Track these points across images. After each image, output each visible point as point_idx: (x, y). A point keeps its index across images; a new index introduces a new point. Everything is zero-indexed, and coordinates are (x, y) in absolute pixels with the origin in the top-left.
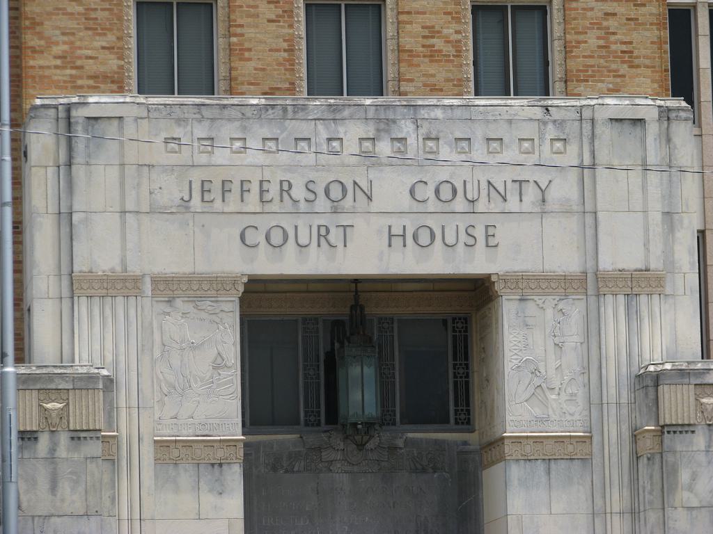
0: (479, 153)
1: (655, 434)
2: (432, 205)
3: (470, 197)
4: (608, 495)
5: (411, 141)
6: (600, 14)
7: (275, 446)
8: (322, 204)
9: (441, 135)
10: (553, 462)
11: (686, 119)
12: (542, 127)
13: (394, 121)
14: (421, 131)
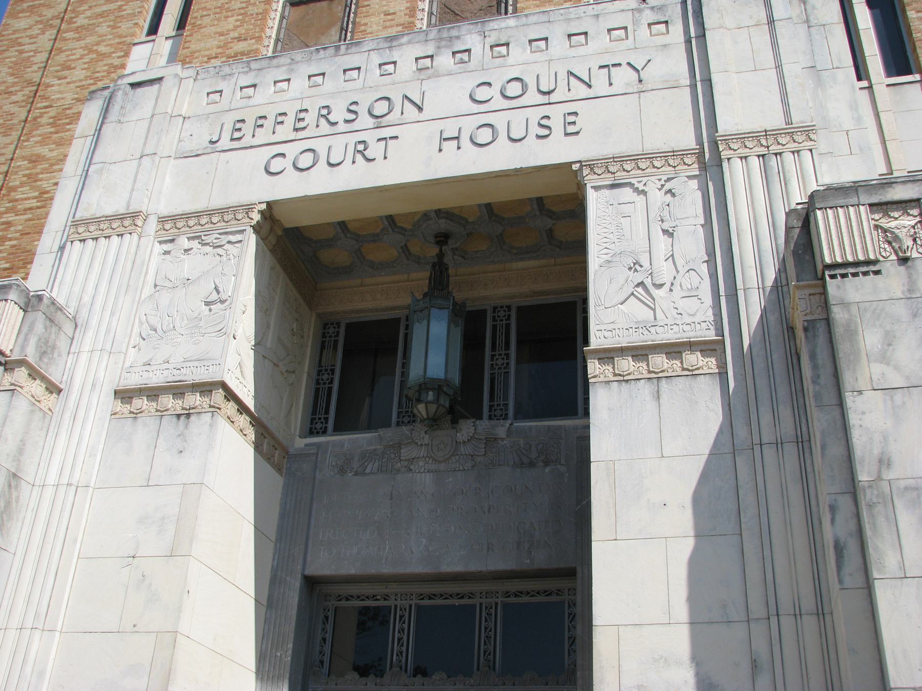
0: (559, 45)
1: (812, 291)
3: (545, 89)
4: (754, 417)
5: (477, 50)
7: (346, 445)
8: (365, 121)
9: (511, 40)
10: (664, 381)
12: (637, 15)
14: (487, 40)
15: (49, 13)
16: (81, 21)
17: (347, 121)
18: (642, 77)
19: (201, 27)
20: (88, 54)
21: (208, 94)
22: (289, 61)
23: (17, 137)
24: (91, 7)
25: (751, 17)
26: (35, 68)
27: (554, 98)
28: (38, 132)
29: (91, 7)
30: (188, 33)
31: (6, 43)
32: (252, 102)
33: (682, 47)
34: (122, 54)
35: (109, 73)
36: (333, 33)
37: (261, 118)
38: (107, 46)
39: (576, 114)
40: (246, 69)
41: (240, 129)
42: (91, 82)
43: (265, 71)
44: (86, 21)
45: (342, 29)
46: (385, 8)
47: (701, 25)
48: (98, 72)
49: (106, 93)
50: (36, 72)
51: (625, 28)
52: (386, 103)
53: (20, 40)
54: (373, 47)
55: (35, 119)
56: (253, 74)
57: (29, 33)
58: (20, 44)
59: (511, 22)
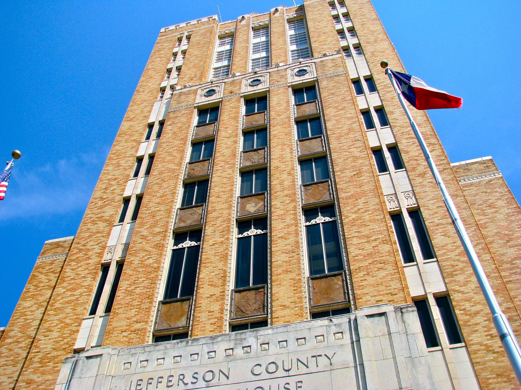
0: (292, 345)
2: (266, 376)
3: (286, 368)
5: (254, 346)
6: (374, 302)
9: (270, 341)
11: (413, 311)
12: (328, 329)
13: (245, 339)
14: (259, 341)
15: (42, 299)
16: (57, 305)
17: (192, 383)
18: (332, 362)
19: (118, 314)
20: (60, 324)
21: (124, 364)
22: (164, 348)
23: (20, 368)
24: (63, 298)
25: (380, 331)
26: (32, 328)
27: (291, 373)
28: (32, 366)
29: (63, 298)
30: (112, 317)
31: (19, 314)
32: (146, 369)
33: (350, 346)
34: (77, 324)
35: (71, 335)
36: (183, 320)
37: (151, 379)
38: (70, 319)
39: (301, 382)
40: (143, 351)
41: (140, 385)
42: (61, 339)
43: (152, 352)
44: (60, 306)
45: (187, 318)
46: (209, 308)
47: (357, 334)
48: (65, 334)
49: (73, 359)
50: (33, 331)
51: (323, 335)
52: (211, 374)
53: (26, 313)
54: (204, 342)
55: (31, 359)
56: (146, 354)
57: (31, 309)
58: (26, 315)
59: (270, 331)
